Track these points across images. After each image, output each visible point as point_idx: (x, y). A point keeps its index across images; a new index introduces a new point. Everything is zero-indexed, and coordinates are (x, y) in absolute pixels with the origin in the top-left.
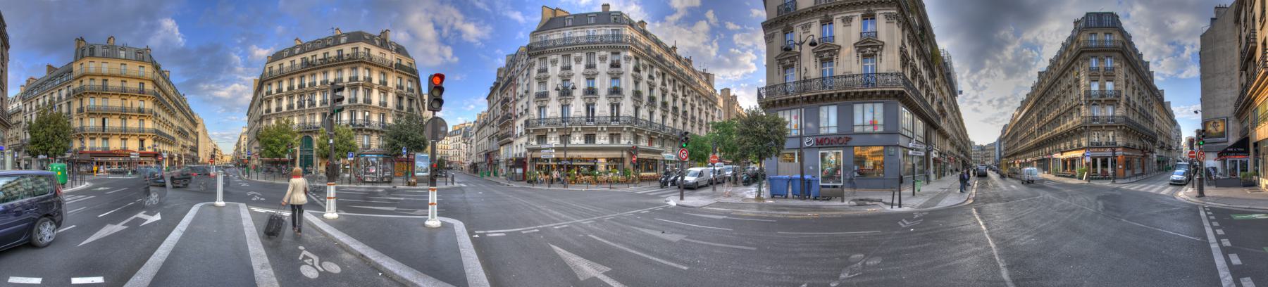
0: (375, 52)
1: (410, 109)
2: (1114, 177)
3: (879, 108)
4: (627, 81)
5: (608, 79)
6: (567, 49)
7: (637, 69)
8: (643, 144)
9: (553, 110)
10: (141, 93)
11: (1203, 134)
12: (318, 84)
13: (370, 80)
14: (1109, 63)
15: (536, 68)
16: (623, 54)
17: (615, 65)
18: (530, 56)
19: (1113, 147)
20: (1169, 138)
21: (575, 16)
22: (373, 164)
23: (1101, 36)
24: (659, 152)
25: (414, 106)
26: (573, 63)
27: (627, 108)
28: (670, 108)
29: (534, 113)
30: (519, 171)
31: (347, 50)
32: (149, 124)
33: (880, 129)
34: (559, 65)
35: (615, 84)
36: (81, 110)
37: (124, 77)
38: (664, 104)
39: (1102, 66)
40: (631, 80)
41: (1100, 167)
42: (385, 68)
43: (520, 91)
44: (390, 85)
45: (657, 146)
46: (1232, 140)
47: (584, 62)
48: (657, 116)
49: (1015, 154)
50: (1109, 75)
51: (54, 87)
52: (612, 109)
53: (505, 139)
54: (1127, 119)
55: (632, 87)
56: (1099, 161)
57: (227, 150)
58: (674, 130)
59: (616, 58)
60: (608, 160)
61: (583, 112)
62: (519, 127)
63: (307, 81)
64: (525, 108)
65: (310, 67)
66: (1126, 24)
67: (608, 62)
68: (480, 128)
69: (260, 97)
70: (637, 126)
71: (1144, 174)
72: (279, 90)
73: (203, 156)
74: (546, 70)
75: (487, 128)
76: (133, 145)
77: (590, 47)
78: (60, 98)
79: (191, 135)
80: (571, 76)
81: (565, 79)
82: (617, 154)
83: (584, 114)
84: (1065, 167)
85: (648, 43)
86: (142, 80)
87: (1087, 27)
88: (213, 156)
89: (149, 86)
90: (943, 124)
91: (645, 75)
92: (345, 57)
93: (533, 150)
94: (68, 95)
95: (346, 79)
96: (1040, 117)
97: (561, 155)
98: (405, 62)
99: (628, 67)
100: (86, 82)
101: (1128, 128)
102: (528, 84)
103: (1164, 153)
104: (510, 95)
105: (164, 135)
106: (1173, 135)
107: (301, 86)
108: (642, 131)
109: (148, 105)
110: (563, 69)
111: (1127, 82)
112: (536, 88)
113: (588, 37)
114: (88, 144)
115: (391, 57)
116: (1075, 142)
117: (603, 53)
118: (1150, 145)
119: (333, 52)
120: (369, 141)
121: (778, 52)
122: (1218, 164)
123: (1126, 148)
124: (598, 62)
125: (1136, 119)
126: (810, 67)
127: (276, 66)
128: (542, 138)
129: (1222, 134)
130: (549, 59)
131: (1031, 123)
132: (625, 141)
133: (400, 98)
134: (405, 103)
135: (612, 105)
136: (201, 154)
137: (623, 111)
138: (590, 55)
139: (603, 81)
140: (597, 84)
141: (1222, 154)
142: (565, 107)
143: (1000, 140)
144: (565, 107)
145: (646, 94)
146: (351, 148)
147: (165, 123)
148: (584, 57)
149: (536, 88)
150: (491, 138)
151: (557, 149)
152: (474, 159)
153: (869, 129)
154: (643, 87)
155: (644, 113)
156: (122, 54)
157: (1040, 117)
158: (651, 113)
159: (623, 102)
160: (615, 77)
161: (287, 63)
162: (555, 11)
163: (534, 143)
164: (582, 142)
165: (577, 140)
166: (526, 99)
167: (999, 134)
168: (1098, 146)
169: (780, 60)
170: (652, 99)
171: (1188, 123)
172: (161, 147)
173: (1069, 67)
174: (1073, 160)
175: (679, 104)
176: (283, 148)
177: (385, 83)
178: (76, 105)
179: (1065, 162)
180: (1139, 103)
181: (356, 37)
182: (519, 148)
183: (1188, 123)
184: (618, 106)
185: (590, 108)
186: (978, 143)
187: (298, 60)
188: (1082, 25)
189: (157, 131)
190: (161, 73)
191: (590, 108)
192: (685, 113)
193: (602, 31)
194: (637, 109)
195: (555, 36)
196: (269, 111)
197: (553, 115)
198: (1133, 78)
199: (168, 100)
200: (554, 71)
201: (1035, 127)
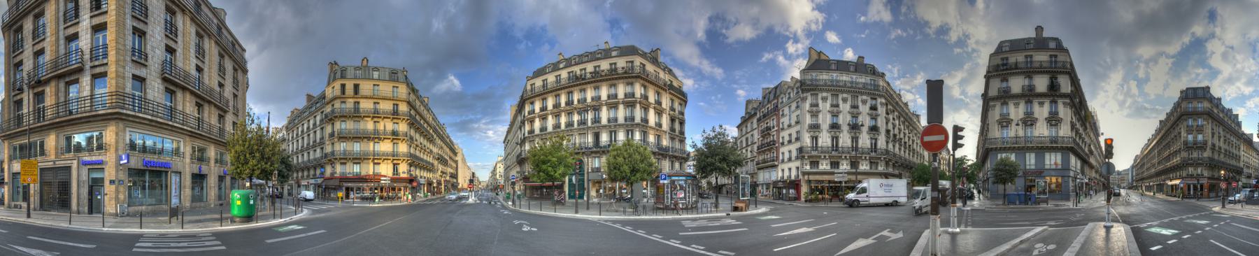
3: (1059, 156)
5: (829, 116)
10: (395, 114)
12: (589, 100)
13: (646, 98)
14: (1200, 122)
19: (1199, 177)
22: (682, 188)
27: (881, 143)
29: (807, 141)
32: (403, 148)
36: (332, 135)
37: (376, 98)
43: (785, 120)
44: (664, 106)
47: (849, 103)
49: (1142, 179)
50: (1200, 130)
51: (311, 114)
57: (484, 177)
63: (576, 97)
65: (579, 82)
67: (868, 105)
69: (520, 117)
72: (544, 109)
73: (463, 181)
76: (385, 169)
77: (855, 91)
78: (315, 124)
79: (450, 162)
80: (839, 112)
86: (394, 100)
88: (471, 181)
89: (403, 108)
90: (1092, 161)
92: (620, 71)
94: (321, 121)
95: (621, 95)
97: (853, 178)
100: (337, 105)
105: (422, 160)
107: (569, 103)
109: (403, 127)
111: (1213, 134)
112: (808, 120)
114: (339, 169)
117: (864, 97)
119: (605, 65)
127: (538, 82)
128: (815, 163)
130: (820, 96)
131: (1153, 158)
136: (460, 180)
137: (879, 145)
138: (855, 97)
143: (1133, 167)
147: (423, 149)
149: (808, 120)
151: (849, 173)
156: (376, 75)
157: (1159, 153)
161: (551, 78)
164: (828, 167)
168: (1192, 176)
172: (417, 173)
176: (561, 170)
178: (328, 129)
182: (788, 170)
185: (835, 139)
187: (564, 74)
189: (411, 155)
190: (419, 97)
191: (835, 139)
193: (863, 79)
195: (824, 76)
196: (532, 132)
199: (421, 123)
201: (1156, 161)
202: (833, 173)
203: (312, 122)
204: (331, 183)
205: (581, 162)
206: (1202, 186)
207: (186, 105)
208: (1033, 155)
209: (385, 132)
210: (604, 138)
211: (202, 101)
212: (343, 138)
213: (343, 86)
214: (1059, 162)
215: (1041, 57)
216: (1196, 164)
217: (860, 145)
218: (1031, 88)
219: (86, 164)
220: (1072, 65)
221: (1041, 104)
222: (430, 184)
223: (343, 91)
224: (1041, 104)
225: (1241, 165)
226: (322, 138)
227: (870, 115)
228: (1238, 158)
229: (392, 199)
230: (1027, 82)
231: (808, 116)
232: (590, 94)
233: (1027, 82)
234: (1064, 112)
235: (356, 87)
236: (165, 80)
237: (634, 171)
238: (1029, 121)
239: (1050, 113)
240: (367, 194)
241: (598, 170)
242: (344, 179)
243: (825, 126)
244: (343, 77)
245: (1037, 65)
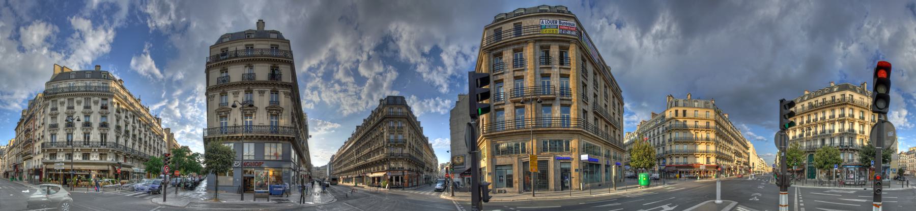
2: (403, 187)
3: (280, 146)
4: (112, 118)
5: (99, 117)
6: (71, 94)
8: (121, 161)
10: (707, 128)
11: (453, 165)
18: (46, 99)
20: (431, 165)
23: (396, 109)
24: (130, 167)
27: (111, 137)
29: (48, 138)
30: (37, 177)
33: (280, 158)
34: (66, 105)
35: (104, 120)
36: (670, 140)
38: (134, 136)
39: (396, 126)
40: (115, 118)
41: (396, 182)
43: (37, 123)
44: (866, 119)
45: (129, 163)
46: (468, 167)
47: (83, 105)
48: (130, 144)
50: (400, 130)
52: (85, 137)
53: (28, 156)
54: (410, 155)
55: (115, 123)
58: (139, 153)
61: (82, 138)
62: (37, 146)
64: (42, 133)
66: (409, 102)
67: (100, 105)
70: (117, 149)
71: (417, 187)
75: (15, 149)
77: (88, 94)
80: (57, 114)
82: (105, 168)
83: (99, 140)
84: (374, 182)
85: (125, 94)
87: (388, 104)
89: (712, 124)
93: (47, 163)
96: (358, 152)
97: (68, 167)
100: (673, 123)
101: (410, 160)
102: (43, 119)
103: (428, 174)
104: (31, 126)
106: (433, 163)
108: (120, 153)
109: (712, 136)
110: (69, 108)
112: (49, 121)
113: (86, 86)
114: (675, 160)
116: (380, 167)
117: (96, 99)
118: (421, 169)
119: (828, 98)
121: (216, 107)
122: (460, 180)
123: (409, 170)
124: (92, 105)
125: (414, 154)
126: (236, 118)
128: (53, 155)
129: (462, 164)
131: (352, 155)
132: (110, 159)
135: (102, 135)
137: (108, 140)
138: (88, 99)
139: (95, 118)
140: (92, 120)
141: (462, 175)
143: (330, 164)
145: (123, 129)
146: (838, 162)
147: (724, 148)
149: (49, 121)
150: (17, 155)
151: (66, 163)
152: (6, 169)
153: (273, 158)
154: (122, 123)
155: (122, 141)
157: (358, 152)
158: (126, 141)
159: (75, 132)
160: (104, 116)
162: (62, 68)
163: (48, 159)
164: (81, 159)
165: (77, 157)
166: (42, 129)
167: (329, 160)
168: (394, 169)
169: (218, 112)
170: (127, 132)
171: (443, 158)
173: (377, 125)
174: (379, 178)
175: (142, 136)
177: (863, 118)
178: (668, 137)
179: (374, 178)
180: (416, 146)
182: (37, 161)
183: (443, 158)
184: (105, 135)
186: (315, 165)
188: (385, 102)
192: (146, 142)
193: (95, 83)
194: (117, 138)
195: (63, 85)
198: (412, 132)
200: (62, 110)
202: (53, 163)
203: (656, 131)
204: (671, 169)
207: (602, 126)
208: (252, 146)
209: (702, 139)
211: (608, 124)
212: (677, 142)
213: (677, 111)
214: (280, 153)
215: (261, 46)
216: (396, 158)
217: (91, 139)
218: (251, 76)
219: (559, 159)
220: (291, 52)
221: (262, 93)
222: (729, 169)
223: (677, 115)
224: (262, 93)
226: (664, 142)
229: (707, 177)
230: (247, 71)
233: (247, 71)
234: (284, 100)
235: (684, 111)
236: (595, 113)
238: (249, 108)
239: (271, 102)
240: (691, 175)
242: (678, 167)
244: (676, 106)
245: (258, 53)
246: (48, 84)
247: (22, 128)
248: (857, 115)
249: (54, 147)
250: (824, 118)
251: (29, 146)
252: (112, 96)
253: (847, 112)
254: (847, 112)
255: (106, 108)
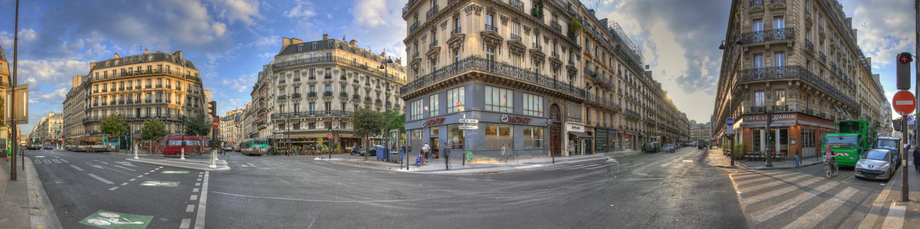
0: (173, 68)
1: (196, 106)
5: (323, 86)
6: (297, 67)
7: (343, 78)
9: (289, 107)
15: (278, 80)
16: (333, 69)
17: (328, 77)
20: (877, 114)
21: (304, 44)
25: (199, 104)
26: (301, 76)
28: (374, 101)
29: (277, 109)
31: (155, 66)
34: (293, 77)
40: (339, 86)
42: (180, 78)
44: (182, 90)
47: (308, 75)
53: (261, 125)
56: (778, 132)
59: (328, 72)
60: (324, 139)
65: (126, 75)
67: (324, 75)
68: (247, 116)
70: (343, 116)
74: (284, 81)
75: (251, 116)
77: (311, 66)
81: (296, 87)
91: (350, 81)
97: (287, 136)
98: (192, 74)
99: (337, 78)
102: (273, 90)
104: (265, 95)
107: (122, 89)
110: (296, 80)
112: (278, 93)
115: (183, 71)
119: (144, 67)
120: (169, 128)
133: (189, 98)
134: (193, 102)
140: (359, 93)
142: (311, 104)
144: (311, 104)
148: (308, 72)
160: (328, 85)
165: (304, 127)
181: (159, 57)
185: (328, 105)
187: (119, 70)
191: (328, 105)
193: (319, 54)
194: (344, 105)
195: (290, 58)
197: (304, 110)
205: (129, 128)
206: (784, 132)
210: (143, 113)
225: (858, 100)
227: (341, 83)
228: (853, 89)
231: (278, 91)
232: (135, 84)
237: (154, 134)
241: (139, 132)
243: (320, 95)
246: (277, 57)
247: (257, 95)
248: (174, 86)
249: (282, 118)
250: (140, 87)
251: (262, 115)
252: (335, 65)
253: (165, 83)
254: (154, 83)
255: (330, 77)
